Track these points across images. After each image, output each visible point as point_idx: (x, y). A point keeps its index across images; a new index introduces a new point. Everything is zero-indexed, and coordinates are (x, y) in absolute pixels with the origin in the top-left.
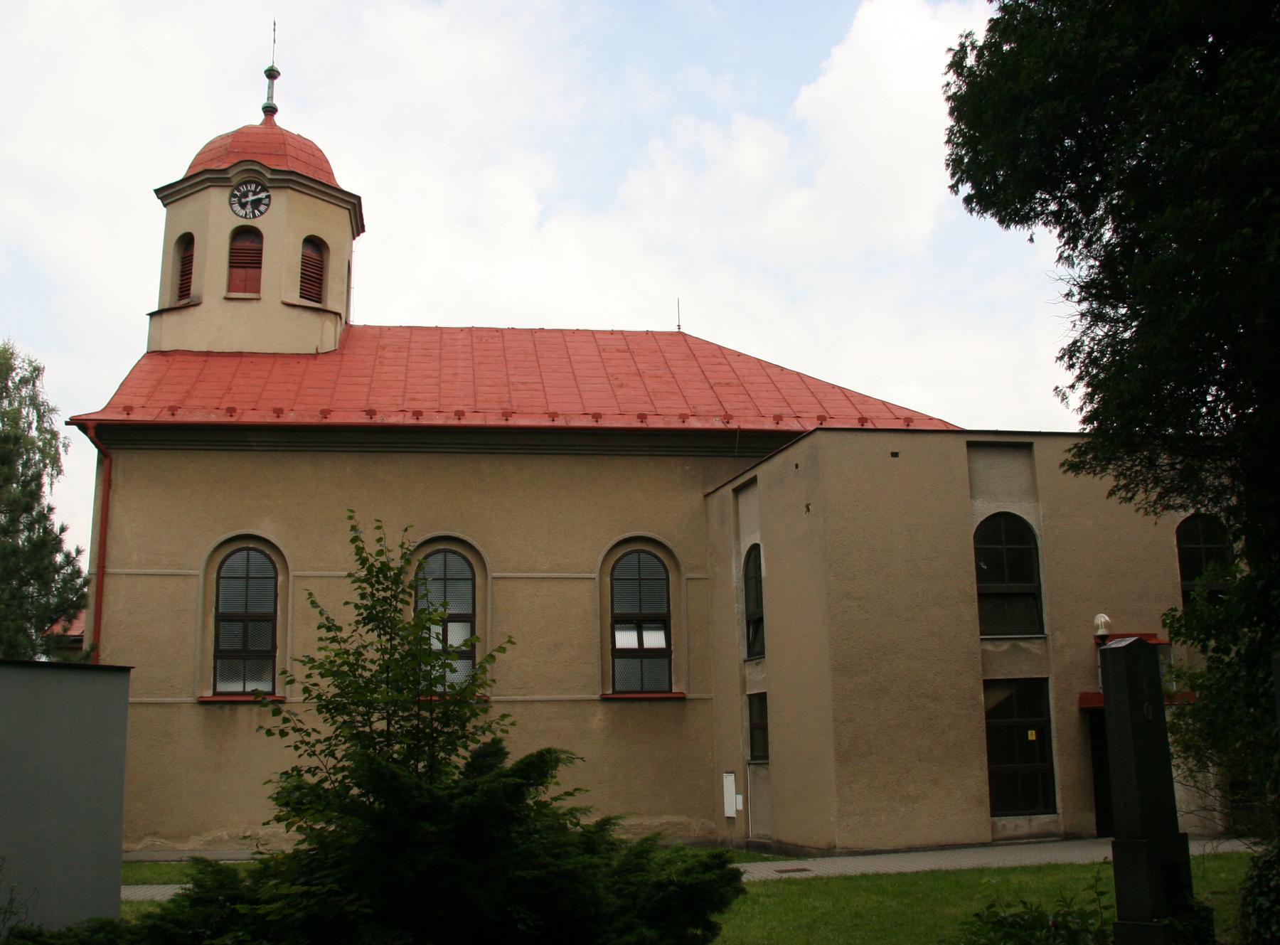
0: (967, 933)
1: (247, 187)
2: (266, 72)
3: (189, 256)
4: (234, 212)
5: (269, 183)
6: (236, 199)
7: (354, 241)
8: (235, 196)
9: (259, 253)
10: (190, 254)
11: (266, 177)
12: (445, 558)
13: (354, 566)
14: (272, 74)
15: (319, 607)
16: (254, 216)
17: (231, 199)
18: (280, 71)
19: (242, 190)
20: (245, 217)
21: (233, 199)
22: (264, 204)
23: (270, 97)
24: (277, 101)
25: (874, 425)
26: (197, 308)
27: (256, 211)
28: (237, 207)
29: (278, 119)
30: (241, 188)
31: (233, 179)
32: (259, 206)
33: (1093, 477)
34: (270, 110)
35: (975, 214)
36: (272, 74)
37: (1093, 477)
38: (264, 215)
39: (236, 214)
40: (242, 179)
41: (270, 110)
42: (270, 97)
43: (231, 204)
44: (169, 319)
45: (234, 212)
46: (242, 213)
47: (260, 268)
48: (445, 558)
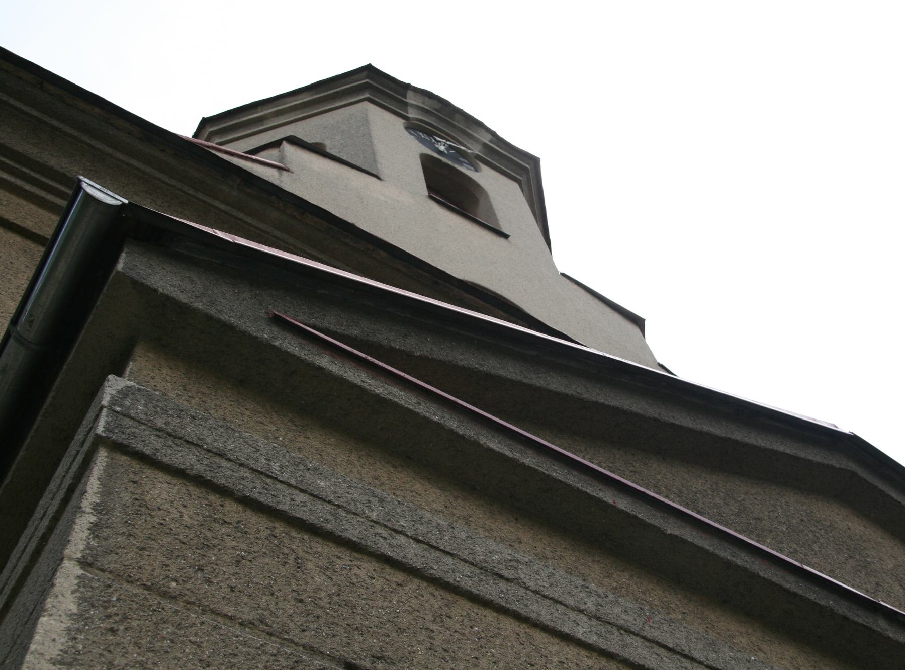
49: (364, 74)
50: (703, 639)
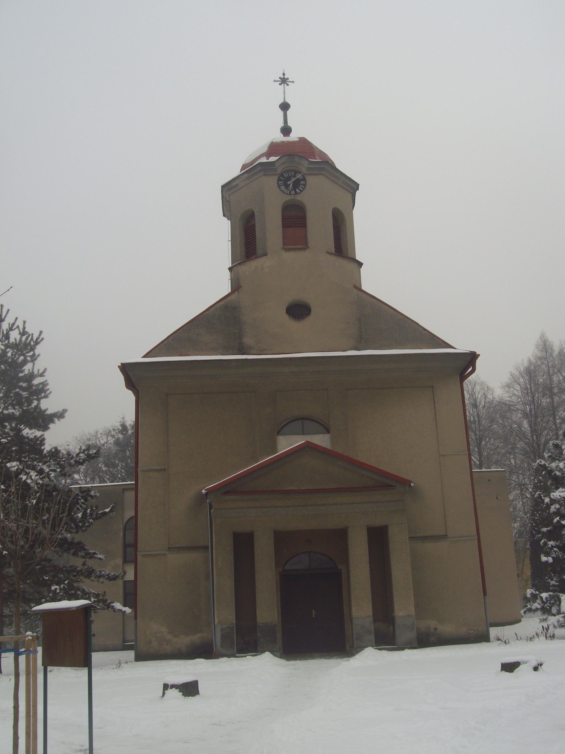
0: (518, 457)
3: (253, 225)
12: (303, 422)
15: (80, 557)
16: (296, 193)
17: (278, 183)
19: (290, 174)
20: (290, 194)
21: (280, 182)
26: (52, 393)
27: (297, 190)
28: (283, 188)
35: (111, 428)
36: (285, 107)
38: (307, 185)
40: (283, 168)
43: (279, 186)
45: (282, 191)
48: (303, 422)
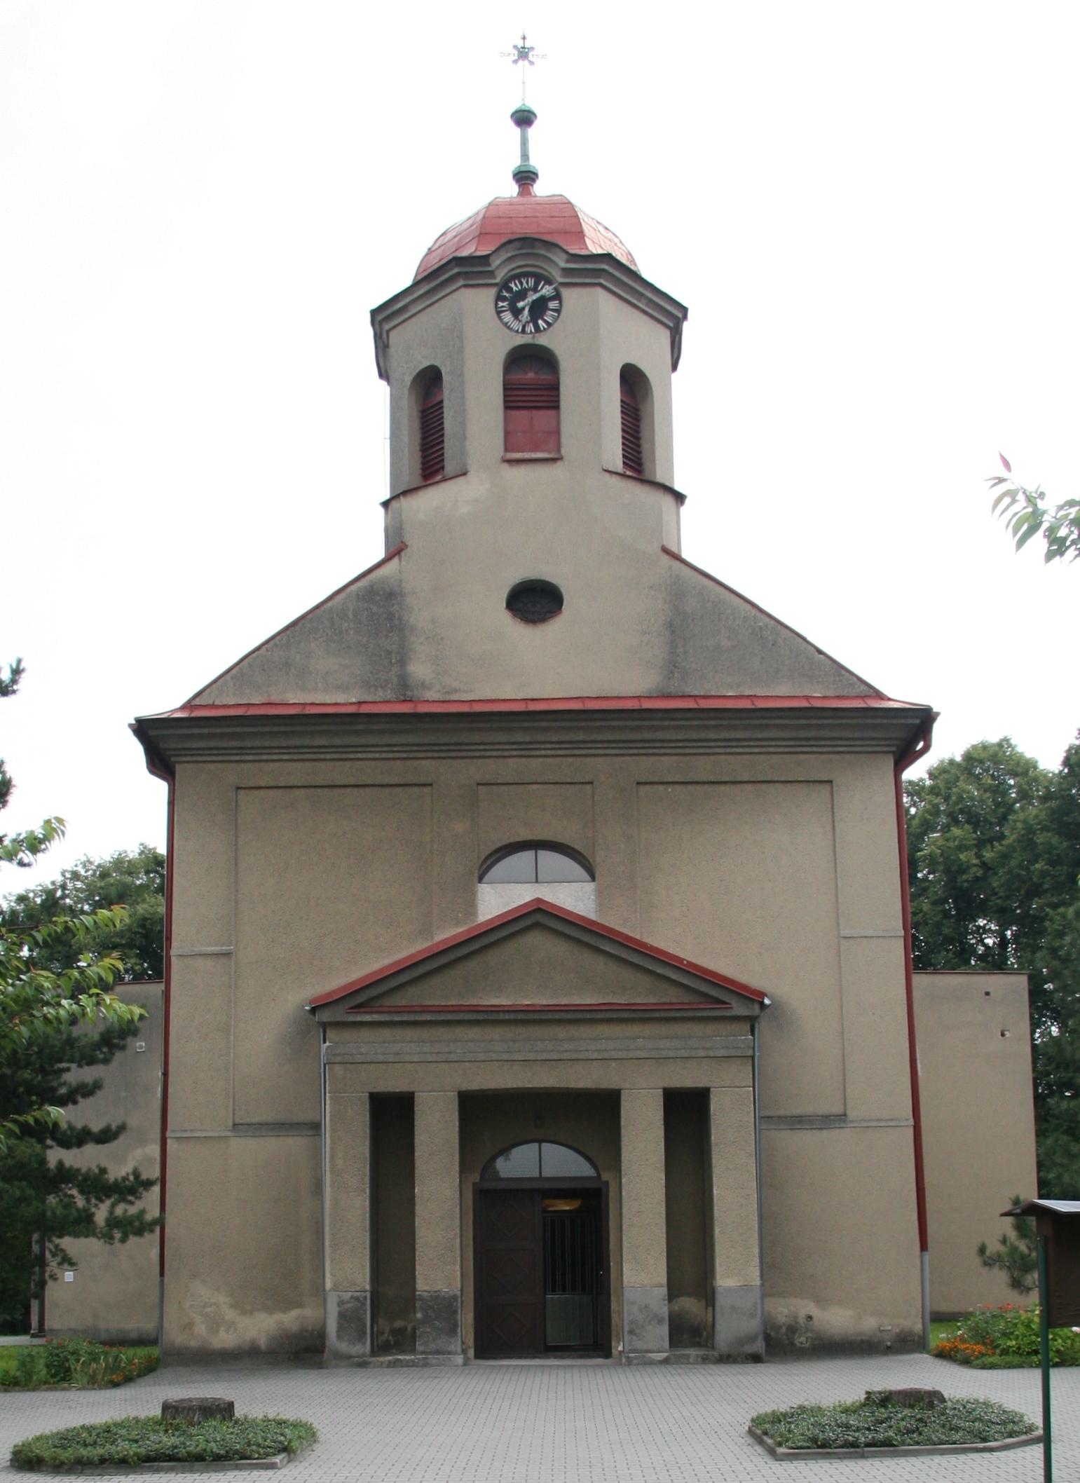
1: (521, 284)
2: (513, 115)
4: (506, 324)
5: (561, 277)
6: (504, 304)
7: (674, 376)
8: (504, 299)
9: (555, 388)
10: (437, 400)
11: (557, 265)
13: (14, 666)
14: (524, 119)
17: (496, 304)
18: (535, 111)
21: (501, 304)
22: (552, 310)
23: (525, 156)
24: (535, 162)
25: (753, 704)
27: (540, 322)
28: (507, 317)
29: (541, 189)
30: (512, 285)
31: (496, 273)
32: (547, 305)
33: (11, 666)
34: (525, 177)
36: (524, 119)
37: (11, 666)
39: (509, 328)
41: (525, 177)
42: (525, 156)
43: (499, 313)
44: (404, 502)
45: (506, 324)
46: (517, 326)
47: (555, 405)
49: (454, 263)
50: (232, 1329)
